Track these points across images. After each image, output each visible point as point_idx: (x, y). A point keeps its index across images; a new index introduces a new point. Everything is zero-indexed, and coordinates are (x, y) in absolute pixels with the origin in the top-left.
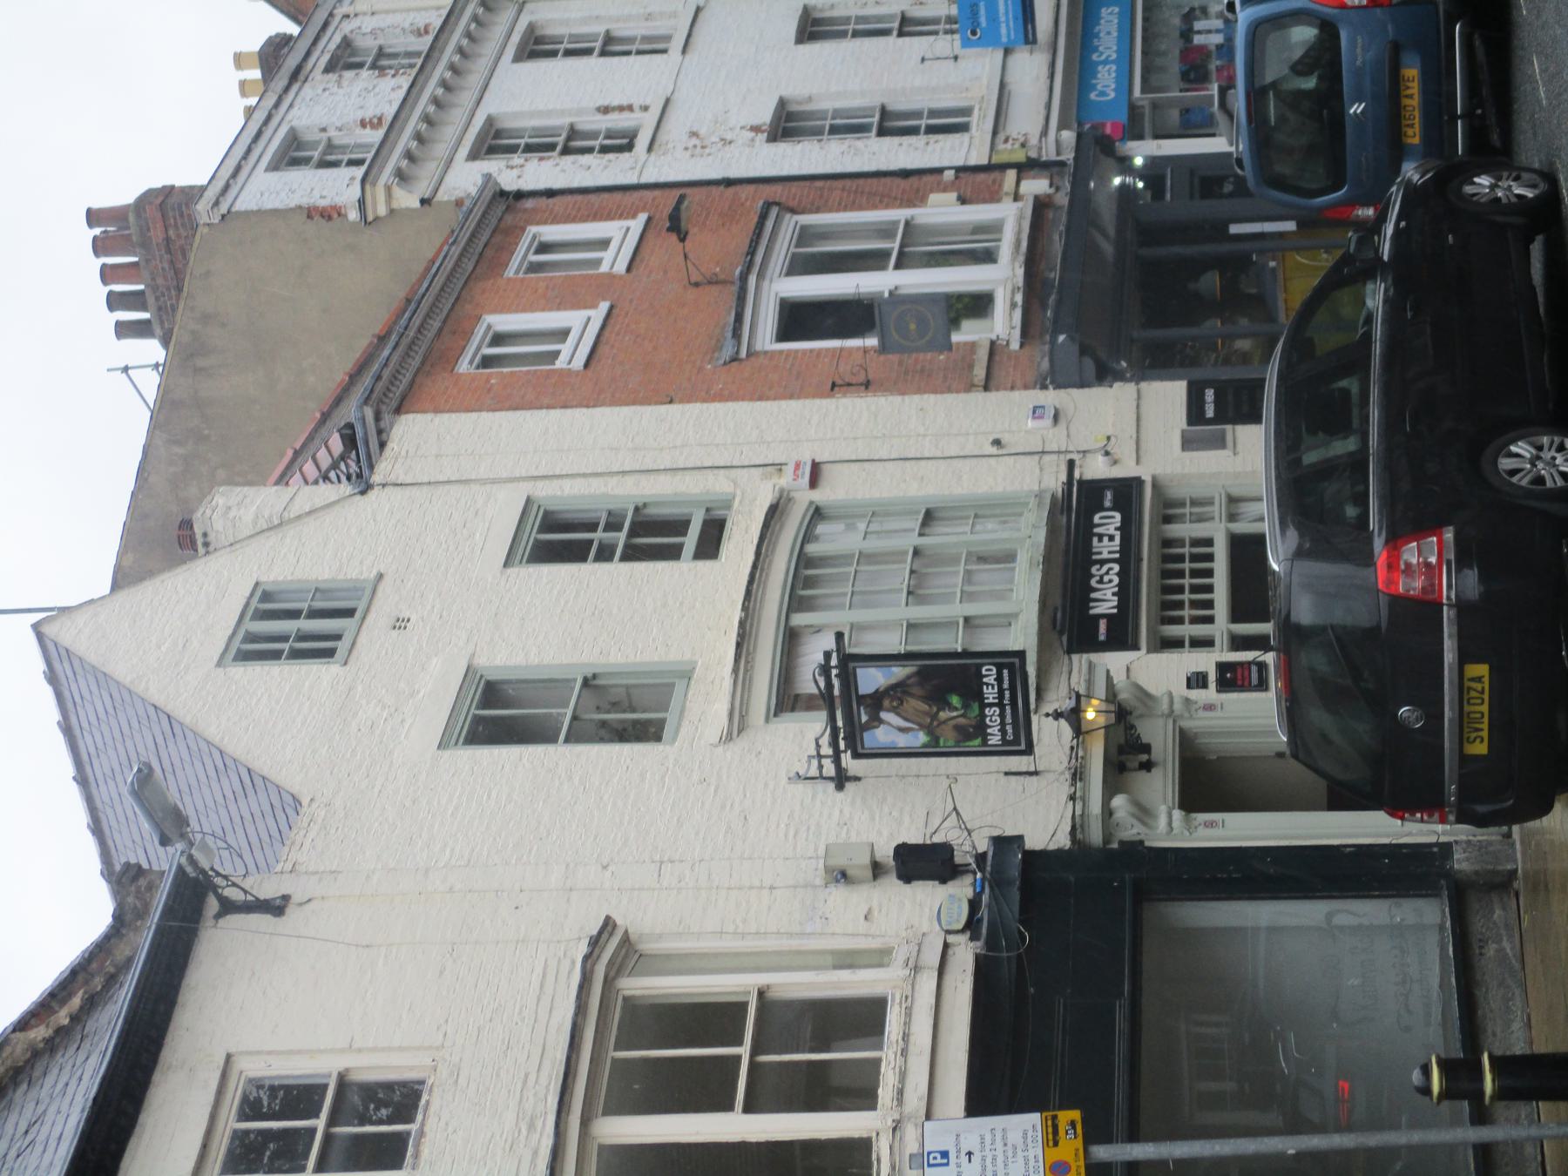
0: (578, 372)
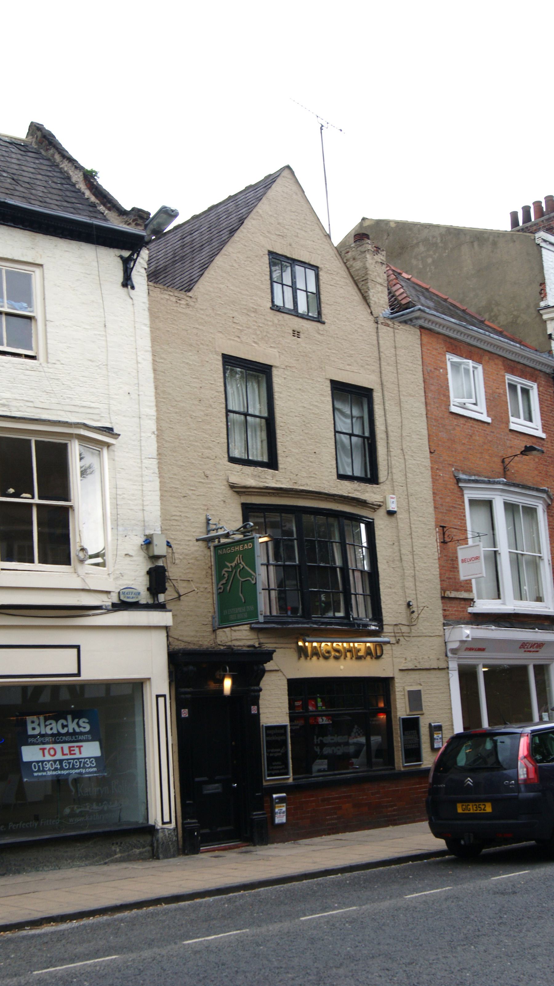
0: (449, 409)
